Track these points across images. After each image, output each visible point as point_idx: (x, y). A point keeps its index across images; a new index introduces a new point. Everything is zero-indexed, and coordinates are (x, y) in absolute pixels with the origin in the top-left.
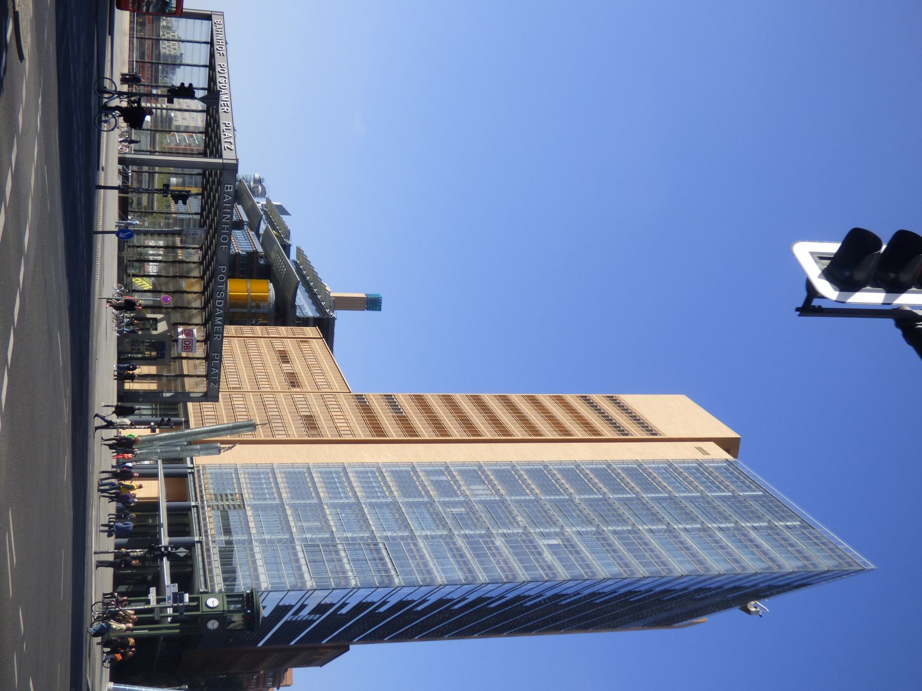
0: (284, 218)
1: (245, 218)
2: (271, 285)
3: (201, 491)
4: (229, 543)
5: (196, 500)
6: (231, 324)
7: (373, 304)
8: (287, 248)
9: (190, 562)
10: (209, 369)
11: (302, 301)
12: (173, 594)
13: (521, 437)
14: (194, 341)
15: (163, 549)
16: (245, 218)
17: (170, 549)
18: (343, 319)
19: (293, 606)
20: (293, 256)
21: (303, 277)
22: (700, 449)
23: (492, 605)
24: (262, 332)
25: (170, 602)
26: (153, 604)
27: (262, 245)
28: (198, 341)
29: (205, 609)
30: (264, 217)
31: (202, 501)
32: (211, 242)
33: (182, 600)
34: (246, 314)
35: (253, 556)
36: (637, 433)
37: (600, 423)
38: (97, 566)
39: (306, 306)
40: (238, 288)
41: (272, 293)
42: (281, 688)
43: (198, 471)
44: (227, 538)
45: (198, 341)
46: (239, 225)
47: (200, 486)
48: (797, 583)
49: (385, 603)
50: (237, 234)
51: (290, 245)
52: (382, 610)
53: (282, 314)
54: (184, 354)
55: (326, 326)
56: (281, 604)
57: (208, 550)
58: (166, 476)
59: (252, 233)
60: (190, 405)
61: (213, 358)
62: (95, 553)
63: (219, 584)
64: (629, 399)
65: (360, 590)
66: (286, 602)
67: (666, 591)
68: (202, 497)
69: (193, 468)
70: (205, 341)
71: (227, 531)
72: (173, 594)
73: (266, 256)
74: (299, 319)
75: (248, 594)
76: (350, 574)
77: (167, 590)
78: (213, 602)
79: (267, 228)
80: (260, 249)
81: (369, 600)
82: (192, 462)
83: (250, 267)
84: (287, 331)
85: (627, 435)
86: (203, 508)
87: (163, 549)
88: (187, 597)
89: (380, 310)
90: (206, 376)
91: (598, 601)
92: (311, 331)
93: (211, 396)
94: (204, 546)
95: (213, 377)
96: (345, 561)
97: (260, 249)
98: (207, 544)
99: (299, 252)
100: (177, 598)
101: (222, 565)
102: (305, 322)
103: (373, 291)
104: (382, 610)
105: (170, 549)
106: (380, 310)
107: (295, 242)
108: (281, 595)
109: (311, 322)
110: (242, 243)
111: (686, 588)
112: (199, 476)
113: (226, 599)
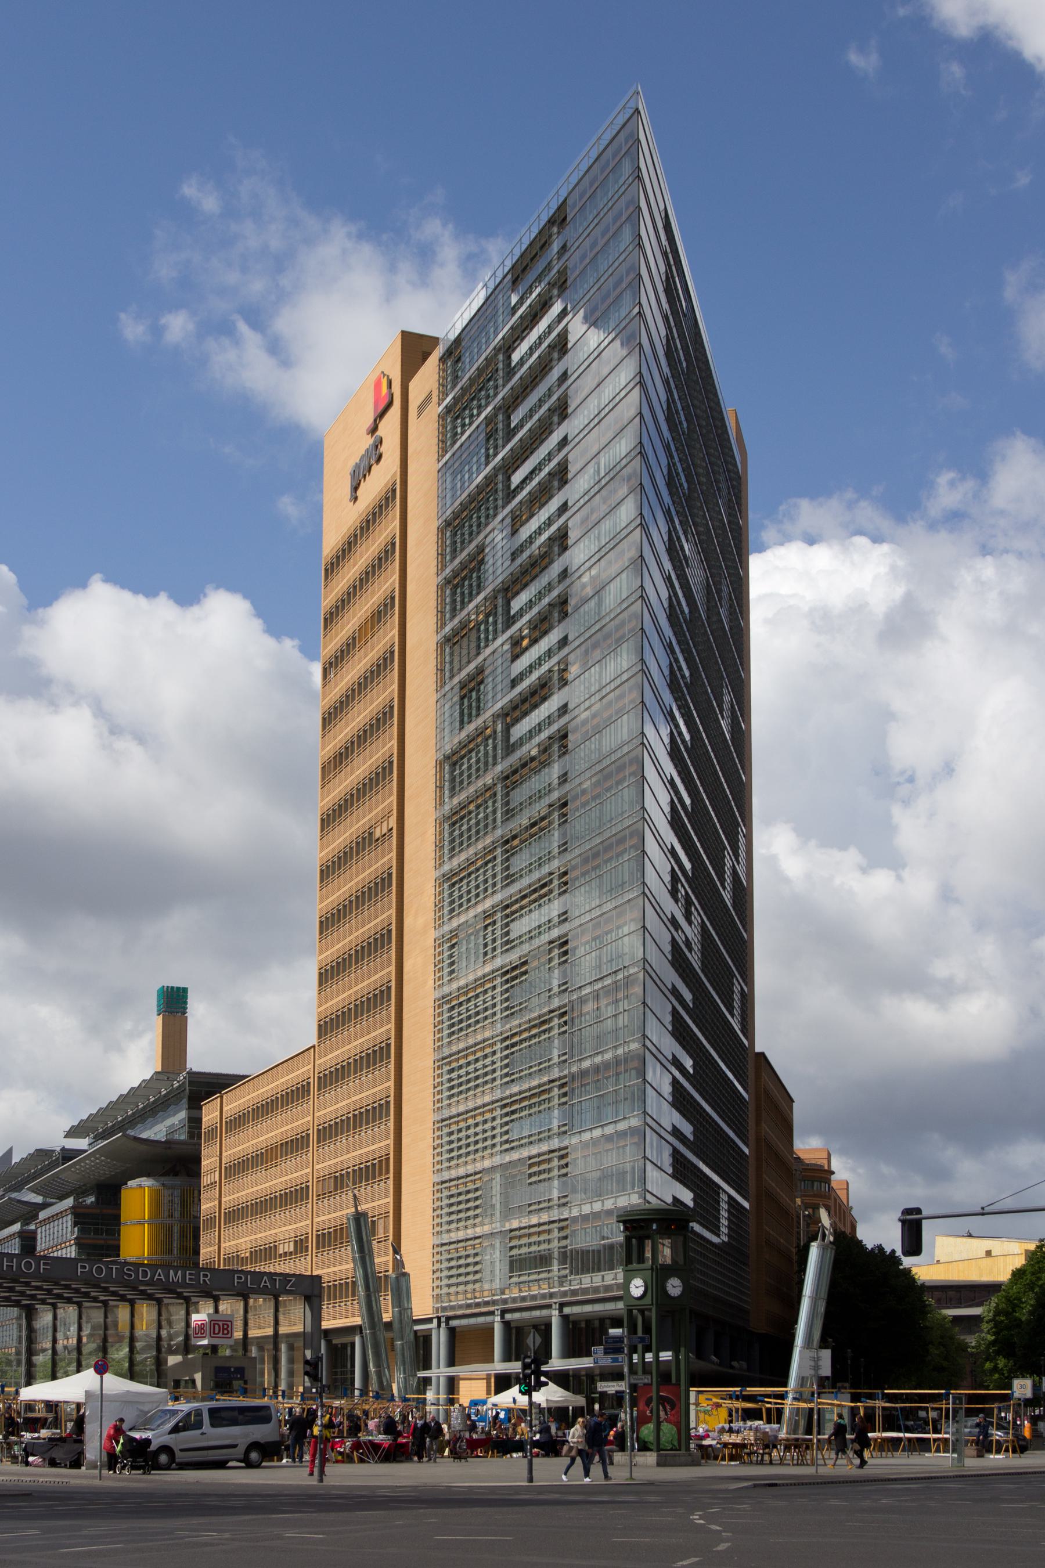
0: (16, 1159)
1: (16, 1227)
2: (130, 1183)
3: (478, 1305)
4: (564, 1256)
5: (492, 1313)
6: (197, 1252)
7: (174, 1003)
8: (67, 1155)
9: (597, 1323)
10: (263, 1292)
11: (157, 1131)
12: (606, 1353)
13: (395, 742)
14: (216, 1317)
15: (528, 1371)
16: (16, 1227)
17: (528, 1360)
18: (201, 1057)
19: (674, 1078)
20: (81, 1143)
21: (121, 1127)
22: (421, 408)
23: (688, 801)
24: (212, 1200)
25: (623, 1358)
26: (620, 1386)
27: (62, 1198)
28: (216, 1311)
29: (648, 1300)
30: (14, 1195)
31: (494, 1303)
32: (38, 1288)
33: (619, 1339)
34: (182, 1229)
35: (585, 1218)
36: (390, 527)
37: (373, 594)
38: (611, 1479)
39: (169, 1122)
40: (137, 1243)
41: (146, 1182)
42: (833, 1168)
43: (444, 1309)
44: (555, 1262)
45: (216, 1311)
46: (28, 1241)
47: (469, 1306)
48: (664, 242)
49: (674, 991)
50: (42, 1246)
51: (63, 1149)
52: (688, 996)
53: (179, 1165)
54: (238, 1334)
55: (210, 1086)
56: (670, 1171)
57: (574, 1293)
58: (451, 1362)
59: (42, 1215)
60: (326, 1325)
61: (243, 1283)
62: (531, 1480)
63: (613, 1277)
64: (331, 540)
65: (649, 1033)
66: (667, 1161)
67: (671, 483)
68: (487, 1303)
69: (439, 1318)
70: (216, 1300)
71: (543, 1260)
72: (606, 1353)
73: (79, 1192)
74: (191, 1135)
75: (626, 1229)
76: (620, 1051)
77: (602, 1363)
78: (637, 1287)
79: (33, 1190)
80: (69, 1202)
81: (668, 1019)
82: (429, 1320)
83: (100, 1223)
84: (209, 1157)
85: (393, 544)
86: (505, 1301)
87: (528, 1371)
88: (614, 1332)
89: (185, 990)
90: (246, 1299)
91: (686, 610)
92: (210, 1114)
93: (311, 1291)
94: (510, 1306)
95: (279, 1288)
96: (598, 1059)
97: (69, 1202)
98: (564, 1294)
99: (72, 1133)
100: (614, 1347)
101: (599, 1270)
102: (195, 1122)
103: (152, 1002)
104: (688, 996)
105: (528, 1360)
106: (185, 990)
107: (56, 1140)
108: (652, 1173)
109: (194, 1113)
110: (59, 1237)
111: (667, 447)
112: (452, 1308)
113: (635, 1266)
